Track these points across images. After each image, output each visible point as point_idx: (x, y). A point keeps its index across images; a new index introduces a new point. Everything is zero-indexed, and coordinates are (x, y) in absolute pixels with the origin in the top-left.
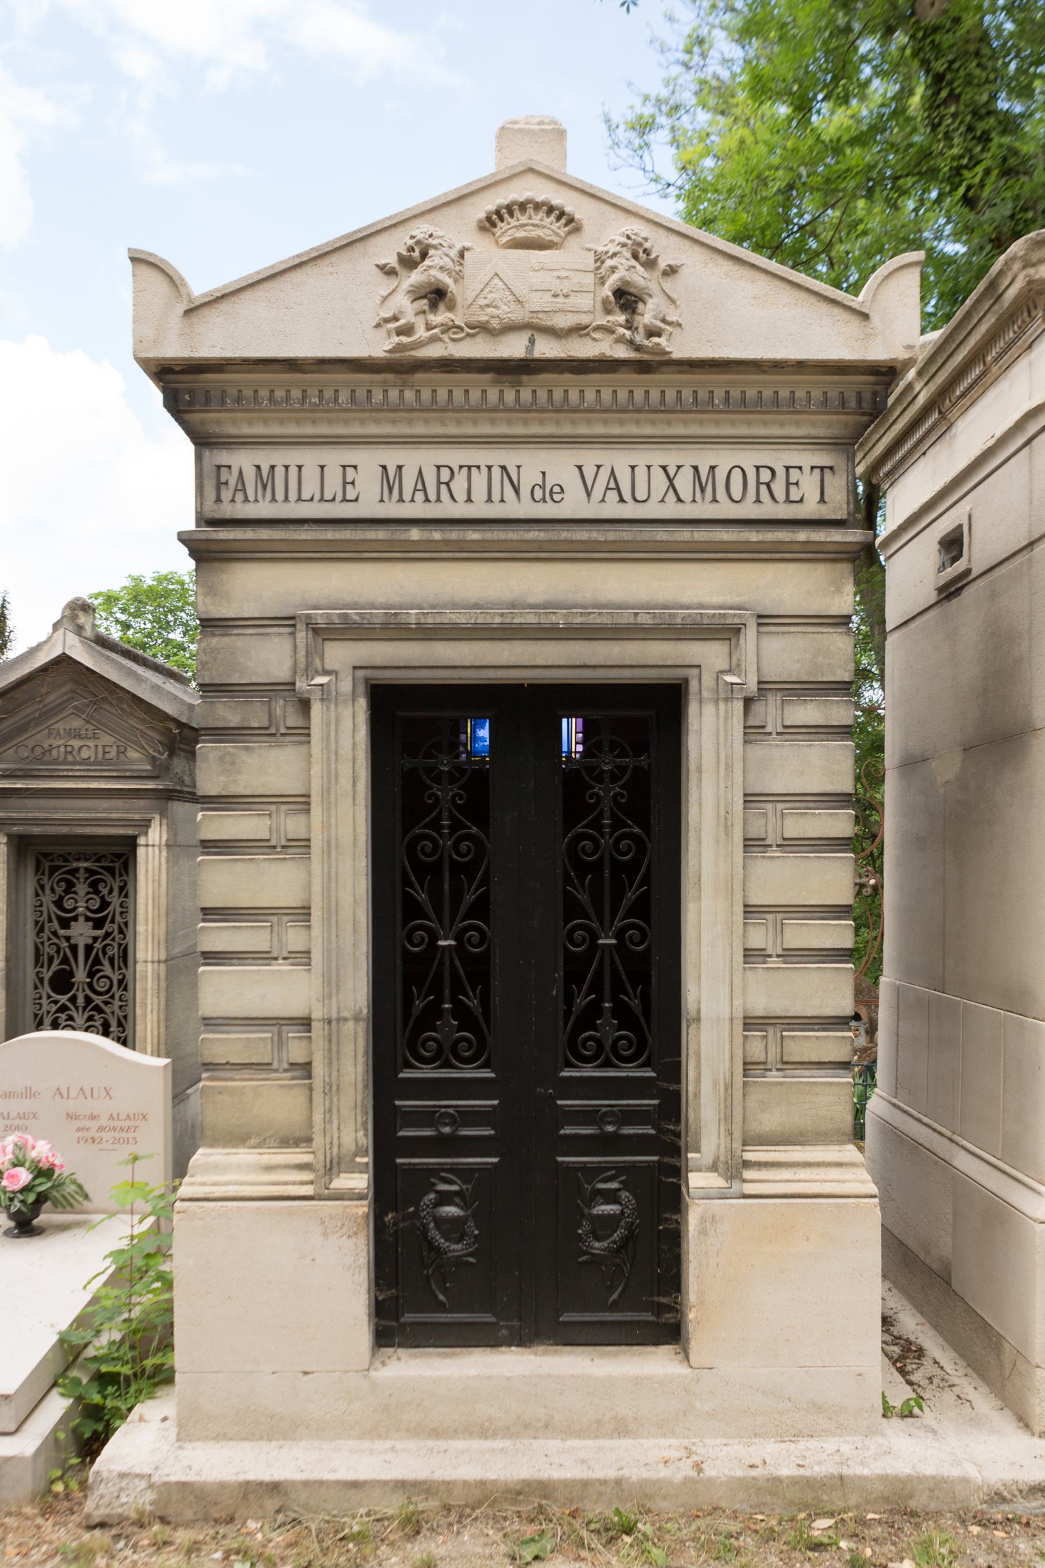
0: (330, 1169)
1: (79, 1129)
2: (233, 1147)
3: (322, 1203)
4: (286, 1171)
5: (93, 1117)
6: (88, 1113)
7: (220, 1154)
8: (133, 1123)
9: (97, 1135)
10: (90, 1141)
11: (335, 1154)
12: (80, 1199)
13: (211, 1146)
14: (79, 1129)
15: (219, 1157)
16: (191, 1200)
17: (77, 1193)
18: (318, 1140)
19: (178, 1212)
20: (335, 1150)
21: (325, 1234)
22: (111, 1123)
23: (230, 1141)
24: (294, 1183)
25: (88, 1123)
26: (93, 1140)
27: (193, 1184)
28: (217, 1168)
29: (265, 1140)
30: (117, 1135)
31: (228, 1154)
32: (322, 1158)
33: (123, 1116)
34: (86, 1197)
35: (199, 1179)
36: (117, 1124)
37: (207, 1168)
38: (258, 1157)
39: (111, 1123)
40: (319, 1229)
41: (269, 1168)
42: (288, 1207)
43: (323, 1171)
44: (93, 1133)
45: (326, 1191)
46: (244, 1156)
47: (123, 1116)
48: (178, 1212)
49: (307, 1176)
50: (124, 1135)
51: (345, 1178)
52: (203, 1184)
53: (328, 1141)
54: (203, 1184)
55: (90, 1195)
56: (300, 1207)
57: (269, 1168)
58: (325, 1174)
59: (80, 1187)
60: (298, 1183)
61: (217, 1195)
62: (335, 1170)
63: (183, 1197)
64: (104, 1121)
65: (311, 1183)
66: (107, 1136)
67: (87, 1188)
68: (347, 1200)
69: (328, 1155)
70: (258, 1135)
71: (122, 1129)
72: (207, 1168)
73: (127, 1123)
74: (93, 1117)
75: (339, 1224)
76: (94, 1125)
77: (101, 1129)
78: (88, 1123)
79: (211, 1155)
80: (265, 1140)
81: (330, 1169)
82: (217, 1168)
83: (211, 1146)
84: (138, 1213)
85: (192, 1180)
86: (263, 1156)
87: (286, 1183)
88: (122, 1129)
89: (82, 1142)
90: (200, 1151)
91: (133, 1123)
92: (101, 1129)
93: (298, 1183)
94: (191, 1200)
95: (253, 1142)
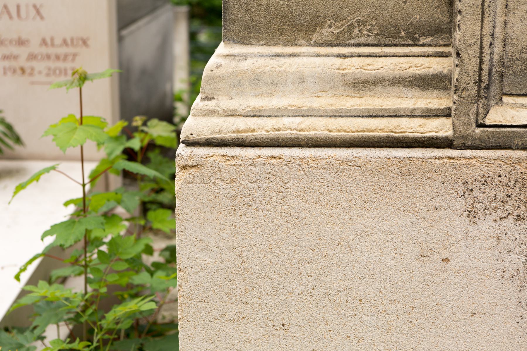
0: (488, 87)
1: (6, 57)
2: (287, 43)
3: (468, 153)
4: (395, 89)
5: (21, 42)
6: (15, 36)
7: (262, 56)
8: (70, 50)
9: (27, 65)
10: (19, 72)
11: (496, 57)
12: (10, 142)
13: (242, 41)
14: (6, 57)
15: (261, 61)
16: (209, 143)
17: (5, 134)
18: (466, 30)
19: (184, 167)
20: (498, 49)
21: (471, 213)
22: (44, 50)
23: (281, 31)
24: (412, 115)
25: (15, 50)
26: (23, 70)
27: (213, 113)
28: (257, 81)
29: (350, 28)
30: (53, 64)
31: (278, 55)
32: (472, 65)
33: (58, 41)
34: (18, 140)
35: (223, 103)
36: (51, 51)
37: (237, 83)
38: (338, 61)
39: (44, 50)
40: (461, 204)
41: (361, 84)
42: (400, 160)
43: (473, 90)
44: (22, 62)
45: (478, 131)
46: (311, 61)
47: (58, 41)
48: (184, 167)
49: (435, 101)
50: (61, 65)
51: (513, 106)
52: (232, 114)
53: (487, 30)
54: (232, 114)
55: (23, 136)
56: (424, 160)
57: (361, 84)
58: (479, 96)
59: (9, 127)
60: (418, 113)
61: (260, 134)
62: (495, 89)
63: (195, 137)
64: (35, 47)
65: (447, 113)
66: (40, 66)
67: (19, 129)
68: (518, 149)
69: (486, 59)
70: (337, 18)
71: (58, 57)
72: (237, 83)
73: (62, 51)
74: (21, 42)
75: (500, 195)
76: (23, 52)
77: (32, 57)
78: (15, 50)
79: (244, 57)
80: (350, 28)
81: (488, 87)
82: (257, 81)
83: (243, 41)
84: (91, 160)
85: (210, 105)
86: (348, 61)
87: (396, 115)
88: (58, 57)
89: (9, 74)
90: (222, 49)
91: (70, 50)
92: (32, 57)
93: (418, 113)
94: (209, 143)
95: (326, 32)
